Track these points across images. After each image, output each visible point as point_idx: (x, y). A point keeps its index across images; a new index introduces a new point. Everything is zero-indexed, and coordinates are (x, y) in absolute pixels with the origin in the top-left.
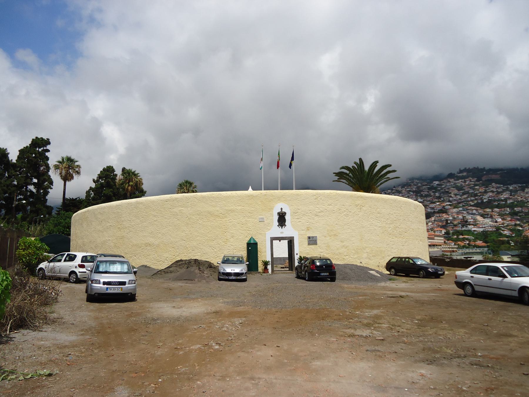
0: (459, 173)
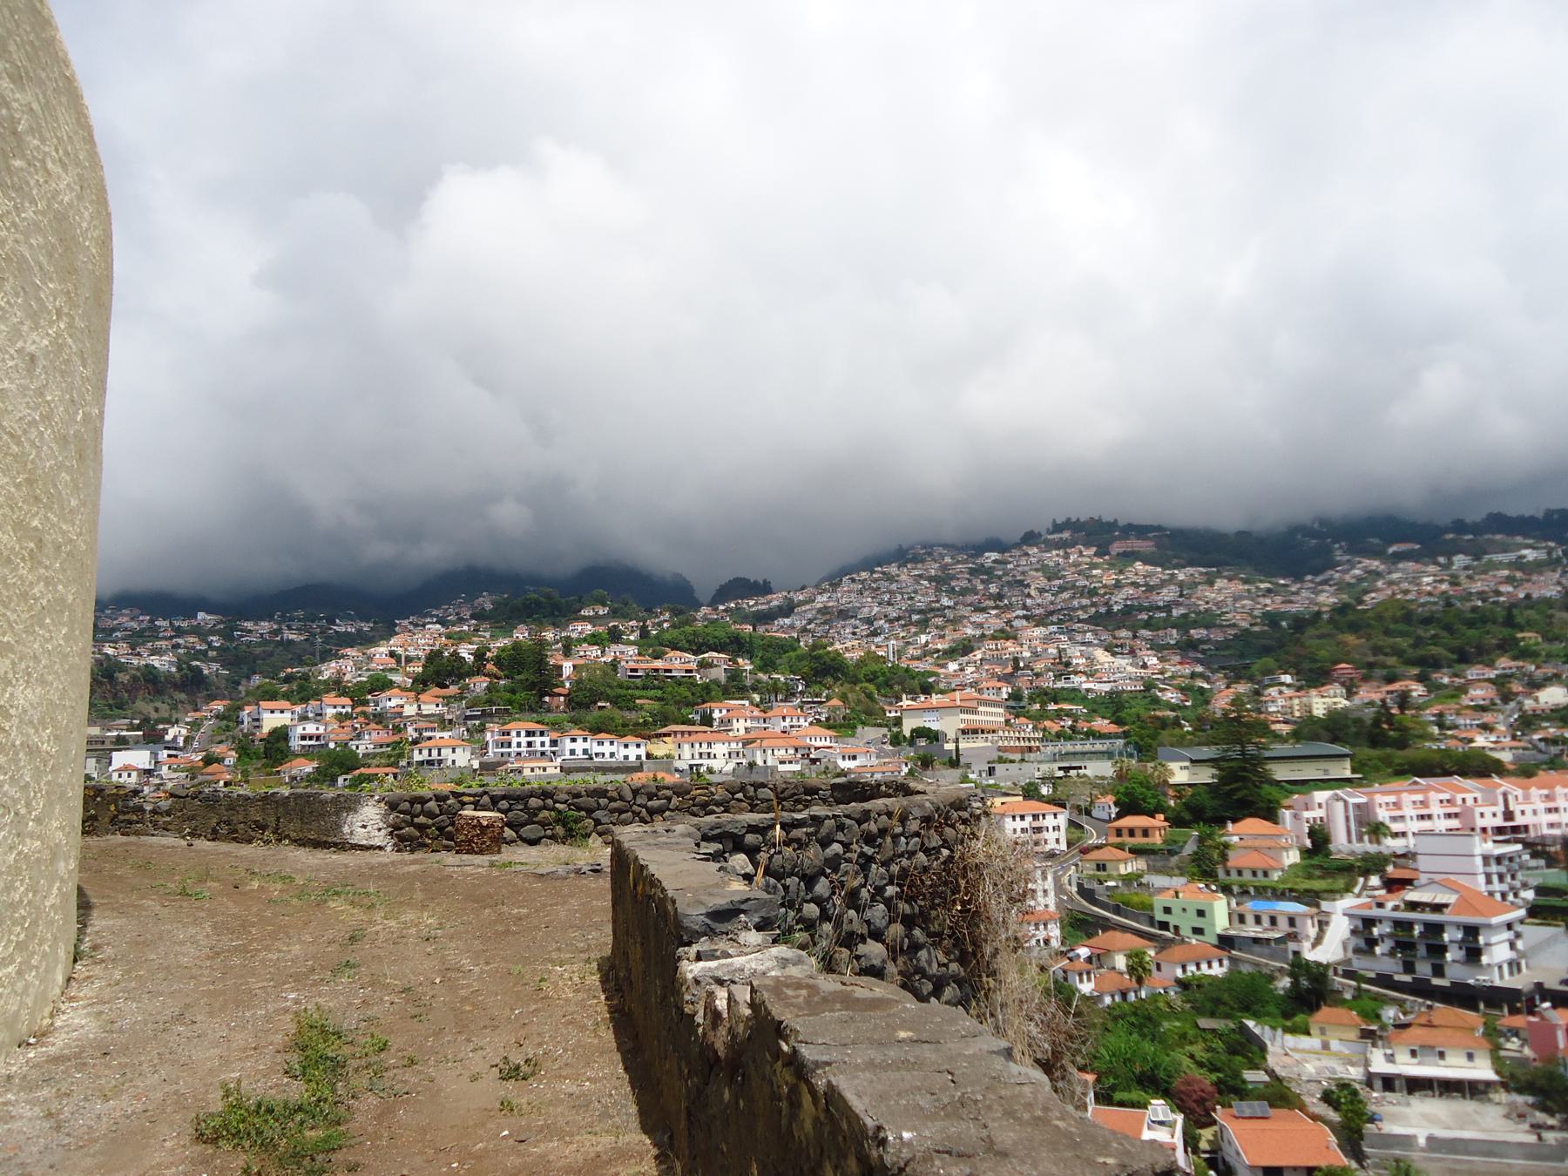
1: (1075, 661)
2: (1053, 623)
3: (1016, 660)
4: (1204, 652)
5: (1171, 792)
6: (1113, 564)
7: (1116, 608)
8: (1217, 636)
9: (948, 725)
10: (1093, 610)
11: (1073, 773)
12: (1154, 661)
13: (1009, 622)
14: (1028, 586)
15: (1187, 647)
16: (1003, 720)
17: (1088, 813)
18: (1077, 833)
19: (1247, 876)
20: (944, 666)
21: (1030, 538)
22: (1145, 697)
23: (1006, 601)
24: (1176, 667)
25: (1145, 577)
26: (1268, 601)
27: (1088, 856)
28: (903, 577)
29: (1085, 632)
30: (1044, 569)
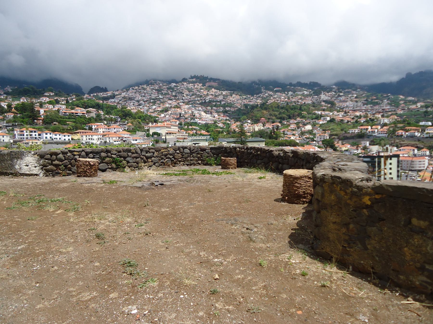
0: (190, 79)
2: (190, 104)
3: (180, 114)
4: (229, 114)
7: (207, 101)
8: (232, 110)
10: (201, 101)
14: (183, 93)
20: (160, 115)
21: (184, 80)
24: (223, 117)
25: (215, 93)
26: (245, 101)
29: (199, 107)
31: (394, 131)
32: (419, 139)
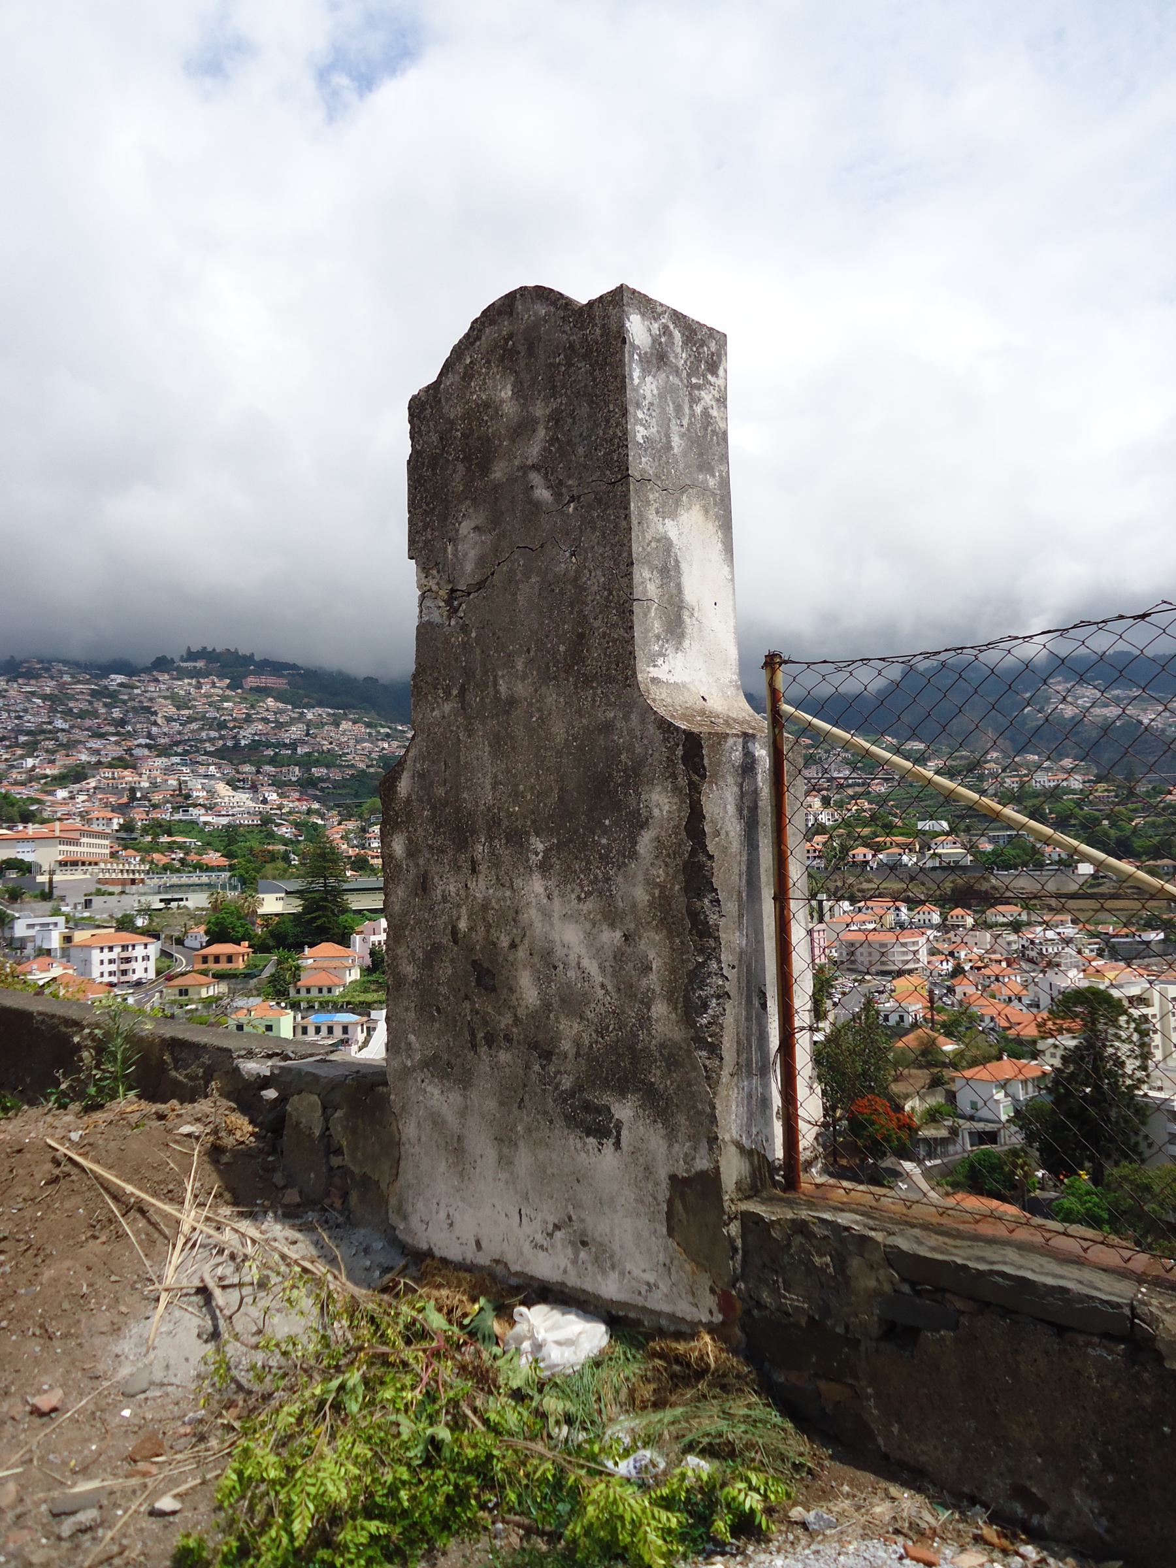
1: (195, 794)
2: (177, 754)
3: (133, 790)
4: (322, 790)
5: (259, 921)
6: (246, 699)
7: (243, 743)
8: (335, 775)
9: (44, 856)
10: (221, 742)
11: (174, 905)
12: (274, 796)
13: (129, 751)
14: (155, 713)
15: (307, 785)
16: (107, 851)
17: (180, 942)
18: (167, 962)
19: (314, 992)
20: (51, 793)
21: (162, 664)
22: (261, 831)
23: (129, 728)
24: (294, 803)
25: (276, 713)
26: (386, 745)
27: (172, 983)
28: (12, 693)
29: (209, 765)
30: (173, 698)
31: (845, 850)
32: (913, 876)
